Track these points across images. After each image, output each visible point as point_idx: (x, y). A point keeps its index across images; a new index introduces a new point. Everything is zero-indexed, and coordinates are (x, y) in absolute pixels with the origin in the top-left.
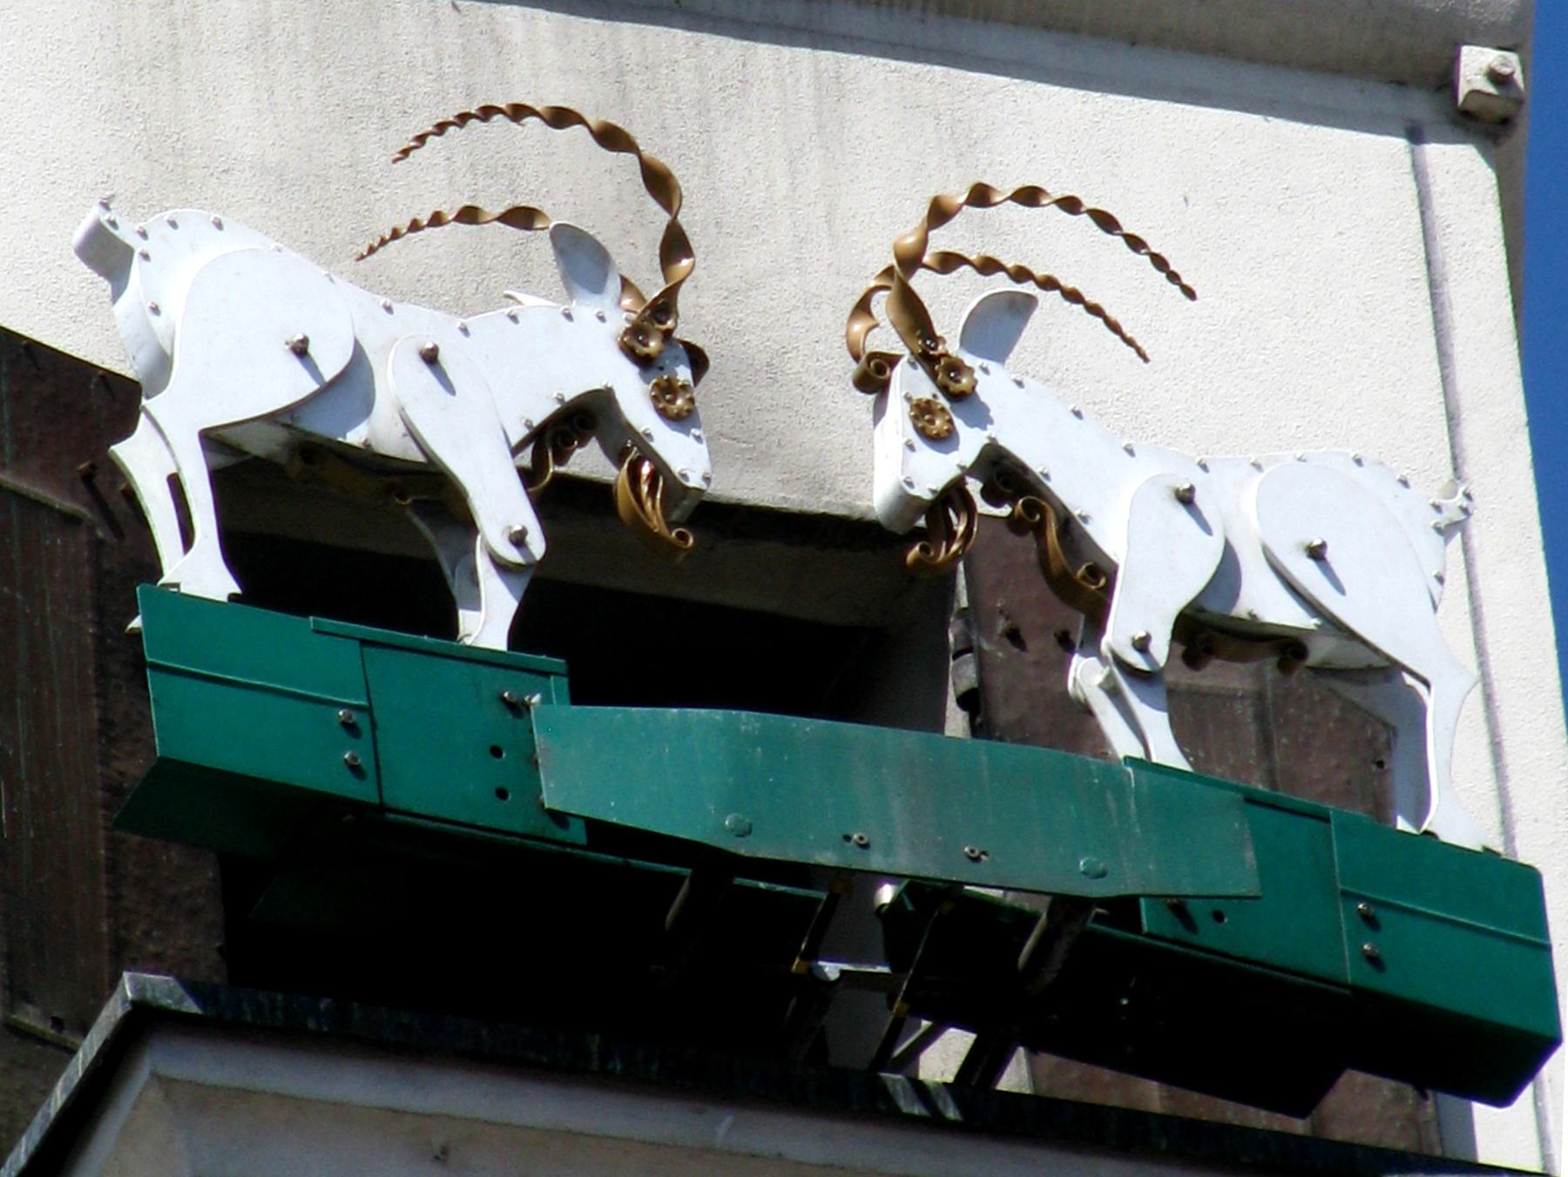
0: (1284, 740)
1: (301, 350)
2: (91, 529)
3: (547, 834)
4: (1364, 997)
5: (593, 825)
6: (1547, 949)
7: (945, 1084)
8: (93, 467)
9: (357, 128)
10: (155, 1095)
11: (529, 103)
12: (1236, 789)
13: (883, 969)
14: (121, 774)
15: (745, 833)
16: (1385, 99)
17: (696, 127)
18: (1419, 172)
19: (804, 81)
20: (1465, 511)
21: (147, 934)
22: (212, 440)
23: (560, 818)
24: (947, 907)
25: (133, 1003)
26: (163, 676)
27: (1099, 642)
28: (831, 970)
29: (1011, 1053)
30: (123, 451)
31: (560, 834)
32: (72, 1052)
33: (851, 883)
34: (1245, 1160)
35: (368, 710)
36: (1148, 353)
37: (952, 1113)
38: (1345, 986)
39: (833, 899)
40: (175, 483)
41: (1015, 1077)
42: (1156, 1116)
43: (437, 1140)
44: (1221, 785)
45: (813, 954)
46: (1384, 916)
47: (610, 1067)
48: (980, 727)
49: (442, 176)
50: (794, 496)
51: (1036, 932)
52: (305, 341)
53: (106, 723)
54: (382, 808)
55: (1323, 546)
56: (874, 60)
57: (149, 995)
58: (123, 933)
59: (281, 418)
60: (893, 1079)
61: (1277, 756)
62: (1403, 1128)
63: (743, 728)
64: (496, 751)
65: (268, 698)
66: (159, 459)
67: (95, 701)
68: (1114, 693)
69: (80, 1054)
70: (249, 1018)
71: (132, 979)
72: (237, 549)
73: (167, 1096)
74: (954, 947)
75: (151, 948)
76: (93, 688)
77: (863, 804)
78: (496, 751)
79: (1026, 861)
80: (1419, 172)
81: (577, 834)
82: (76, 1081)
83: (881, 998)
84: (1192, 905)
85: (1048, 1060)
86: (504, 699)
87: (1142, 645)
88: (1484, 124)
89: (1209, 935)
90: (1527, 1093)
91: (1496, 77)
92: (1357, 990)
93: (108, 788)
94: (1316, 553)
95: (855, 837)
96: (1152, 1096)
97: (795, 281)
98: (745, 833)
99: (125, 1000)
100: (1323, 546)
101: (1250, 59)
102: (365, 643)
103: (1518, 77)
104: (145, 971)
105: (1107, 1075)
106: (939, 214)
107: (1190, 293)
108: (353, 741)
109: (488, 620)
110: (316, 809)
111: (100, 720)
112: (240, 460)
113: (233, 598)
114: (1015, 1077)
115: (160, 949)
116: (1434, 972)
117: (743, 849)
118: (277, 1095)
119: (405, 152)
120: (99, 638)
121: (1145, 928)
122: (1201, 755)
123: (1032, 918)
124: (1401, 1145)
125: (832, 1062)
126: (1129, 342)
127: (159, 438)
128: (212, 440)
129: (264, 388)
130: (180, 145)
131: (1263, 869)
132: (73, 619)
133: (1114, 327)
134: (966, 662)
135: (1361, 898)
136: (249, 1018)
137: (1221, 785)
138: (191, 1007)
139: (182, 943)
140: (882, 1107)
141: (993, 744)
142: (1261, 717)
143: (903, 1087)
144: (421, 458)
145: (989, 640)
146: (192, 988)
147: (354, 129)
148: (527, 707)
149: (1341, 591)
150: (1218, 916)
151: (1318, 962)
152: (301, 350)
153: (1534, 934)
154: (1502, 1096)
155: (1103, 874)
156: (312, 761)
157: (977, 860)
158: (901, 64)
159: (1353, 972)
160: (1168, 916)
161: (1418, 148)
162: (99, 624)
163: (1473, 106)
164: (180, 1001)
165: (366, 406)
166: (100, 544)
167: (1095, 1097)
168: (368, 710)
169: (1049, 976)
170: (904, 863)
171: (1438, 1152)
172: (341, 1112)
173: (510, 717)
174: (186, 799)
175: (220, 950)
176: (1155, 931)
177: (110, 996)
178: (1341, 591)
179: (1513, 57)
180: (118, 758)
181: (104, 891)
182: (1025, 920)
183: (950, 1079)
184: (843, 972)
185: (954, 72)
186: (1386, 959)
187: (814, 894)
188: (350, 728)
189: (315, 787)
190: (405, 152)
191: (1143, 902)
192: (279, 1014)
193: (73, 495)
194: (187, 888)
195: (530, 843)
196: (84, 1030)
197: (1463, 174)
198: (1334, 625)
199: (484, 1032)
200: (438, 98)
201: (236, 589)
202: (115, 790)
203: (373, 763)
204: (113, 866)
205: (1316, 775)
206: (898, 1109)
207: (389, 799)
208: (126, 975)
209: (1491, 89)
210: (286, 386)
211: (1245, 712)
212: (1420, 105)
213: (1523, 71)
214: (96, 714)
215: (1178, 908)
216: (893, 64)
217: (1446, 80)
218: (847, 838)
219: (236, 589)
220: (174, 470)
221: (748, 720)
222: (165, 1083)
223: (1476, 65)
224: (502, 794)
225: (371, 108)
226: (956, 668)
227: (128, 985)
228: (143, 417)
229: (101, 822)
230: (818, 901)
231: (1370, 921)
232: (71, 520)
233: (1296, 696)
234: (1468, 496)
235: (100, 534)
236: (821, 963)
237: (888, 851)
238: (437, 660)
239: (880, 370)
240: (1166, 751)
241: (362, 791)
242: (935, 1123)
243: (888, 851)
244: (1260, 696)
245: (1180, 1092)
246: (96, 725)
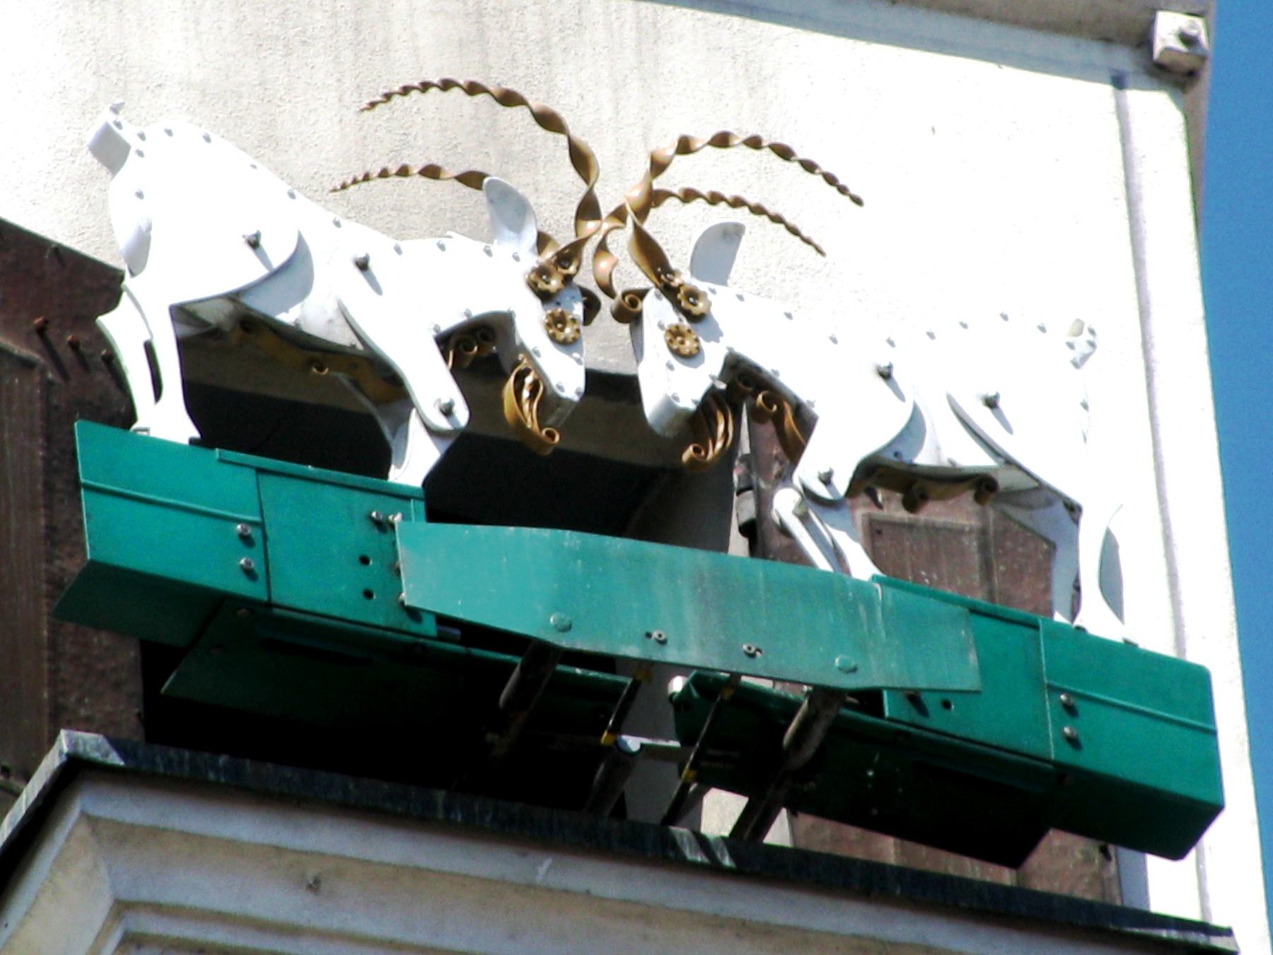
0: (1002, 568)
1: (254, 244)
2: (43, 372)
3: (404, 627)
4: (1063, 772)
5: (442, 620)
6: (1214, 733)
7: (723, 838)
8: (46, 322)
9: (264, 54)
10: (83, 831)
11: (484, 83)
12: (962, 603)
13: (675, 744)
14: (63, 570)
15: (567, 629)
16: (1096, 52)
17: (539, 61)
18: (1122, 113)
19: (627, 26)
20: (1092, 345)
21: (80, 701)
22: (181, 313)
23: (414, 613)
24: (727, 694)
25: (68, 755)
26: (93, 496)
28: (633, 743)
29: (778, 812)
30: (109, 322)
31: (414, 627)
32: (17, 795)
33: (651, 672)
34: (963, 904)
35: (261, 525)
37: (727, 862)
38: (1049, 761)
39: (636, 685)
40: (149, 349)
41: (779, 833)
42: (891, 867)
43: (311, 874)
44: (947, 600)
45: (617, 730)
46: (1082, 706)
47: (453, 816)
48: (757, 548)
49: (333, 94)
50: (611, 361)
51: (799, 715)
52: (257, 236)
53: (51, 529)
54: (269, 605)
55: (997, 397)
56: (685, 10)
57: (81, 749)
58: (61, 700)
59: (234, 297)
60: (680, 831)
61: (996, 580)
62: (1090, 884)
63: (566, 544)
64: (364, 560)
65: (183, 517)
66: (138, 330)
67: (42, 511)
68: (804, 519)
69: (24, 796)
70: (161, 770)
71: (67, 736)
72: (199, 400)
73: (94, 832)
74: (735, 729)
75: (83, 712)
76: (41, 501)
77: (645, 607)
78: (364, 560)
79: (792, 659)
80: (1122, 113)
81: (429, 627)
82: (20, 818)
83: (673, 767)
84: (924, 696)
85: (806, 821)
86: (371, 518)
87: (827, 480)
88: (1175, 76)
89: (938, 720)
90: (1192, 854)
91: (1188, 40)
92: (1057, 765)
93: (49, 582)
94: (991, 403)
95: (655, 635)
96: (888, 850)
97: (617, 186)
98: (567, 629)
99: (61, 753)
100: (997, 397)
101: (988, 18)
102: (260, 471)
103: (1203, 38)
104: (78, 730)
105: (853, 832)
107: (858, 201)
108: (246, 550)
109: (416, 461)
110: (213, 607)
111: (47, 527)
112: (205, 330)
113: (193, 442)
114: (779, 833)
115: (90, 713)
116: (1120, 749)
117: (565, 642)
118: (182, 833)
119: (373, 105)
120: (47, 461)
121: (887, 714)
122: (935, 577)
123: (797, 705)
124: (1089, 897)
125: (631, 815)
127: (136, 311)
128: (181, 313)
129: (208, 269)
130: (121, 65)
131: (983, 669)
132: (27, 444)
134: (748, 498)
135: (1062, 691)
136: (161, 770)
137: (947, 600)
138: (115, 759)
139: (108, 708)
140: (671, 854)
141: (768, 562)
142: (984, 548)
143: (689, 839)
145: (766, 480)
146: (117, 745)
147: (264, 54)
148: (392, 526)
149: (1009, 429)
150: (947, 705)
151: (1028, 743)
152: (254, 244)
153: (1206, 721)
154: (1176, 848)
155: (854, 670)
156: (216, 567)
157: (753, 656)
158: (708, 15)
159: (1055, 751)
160: (907, 705)
161: (1120, 92)
162: (47, 449)
163: (1166, 60)
164: (107, 755)
165: (304, 290)
166: (50, 383)
167: (843, 851)
168: (261, 525)
169: (809, 750)
170: (693, 656)
171: (1118, 903)
172: (233, 847)
173: (376, 531)
174: (114, 593)
175: (139, 715)
176: (895, 716)
177: (49, 750)
178: (1009, 429)
179: (1199, 22)
180: (61, 558)
181: (46, 666)
182: (789, 707)
183: (726, 834)
184: (642, 745)
185: (749, 22)
186: (1083, 740)
187: (621, 679)
188: (246, 539)
189: (211, 585)
190: (373, 105)
191: (885, 694)
192: (187, 768)
193: (30, 347)
194: (113, 664)
195: (389, 634)
196: (27, 777)
197: (1158, 114)
198: (1009, 462)
199: (351, 786)
200: (332, 32)
202: (56, 583)
203: (263, 569)
204: (53, 645)
205: (1027, 596)
206: (684, 857)
207: (276, 598)
208: (63, 733)
209: (1180, 47)
210: (242, 271)
211: (972, 544)
212: (1123, 59)
213: (1208, 34)
214: (43, 522)
215: (914, 698)
216: (700, 14)
217: (1144, 40)
218: (649, 635)
219: (195, 434)
220: (147, 338)
221: (570, 538)
222: (92, 821)
223: (1168, 29)
224: (368, 594)
225: (277, 38)
226: (739, 502)
227: (64, 741)
228: (125, 295)
229: (45, 609)
230: (623, 685)
231: (1070, 710)
232: (27, 364)
233: (973, 522)
234: (1092, 332)
235: (50, 376)
236: (624, 737)
237: (682, 646)
238: (319, 487)
240: (862, 567)
241: (254, 590)
242: (713, 869)
243: (682, 646)
244: (983, 532)
245: (910, 845)
246: (42, 531)
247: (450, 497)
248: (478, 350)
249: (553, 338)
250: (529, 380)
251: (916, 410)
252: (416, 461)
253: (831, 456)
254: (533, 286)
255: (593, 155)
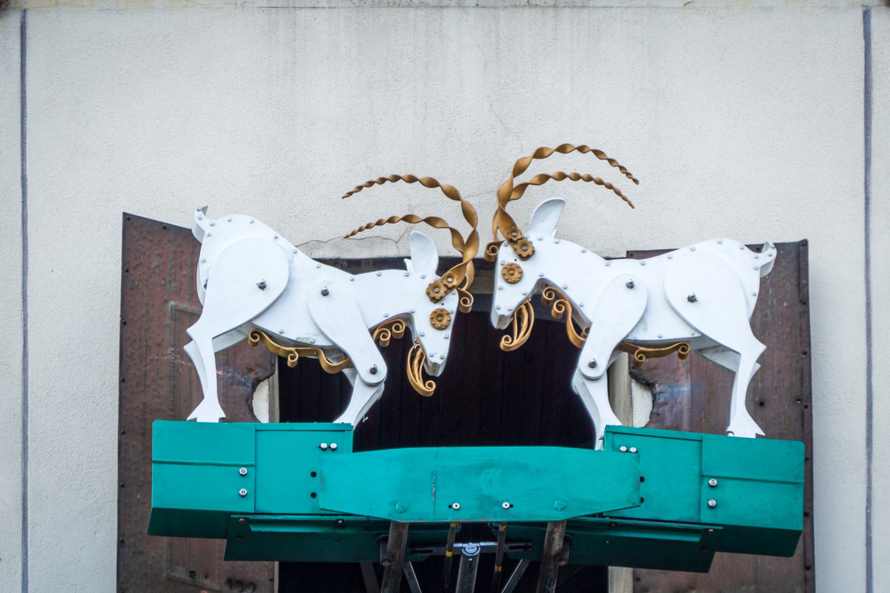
27: (327, 373)
36: (634, 203)
87: (593, 365)
106: (519, 170)
107: (636, 181)
109: (352, 414)
113: (222, 420)
119: (350, 194)
126: (625, 199)
133: (618, 193)
144: (330, 344)
190: (350, 194)
201: (224, 416)
219: (224, 416)
239: (494, 251)
247: (372, 435)
248: (396, 342)
249: (433, 325)
250: (418, 353)
251: (747, 246)
252: (352, 414)
253: (596, 351)
254: (428, 294)
255: (476, 214)
